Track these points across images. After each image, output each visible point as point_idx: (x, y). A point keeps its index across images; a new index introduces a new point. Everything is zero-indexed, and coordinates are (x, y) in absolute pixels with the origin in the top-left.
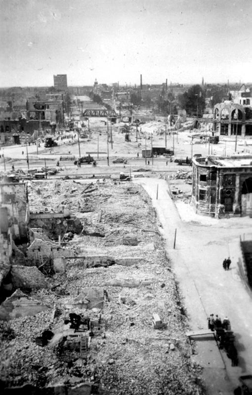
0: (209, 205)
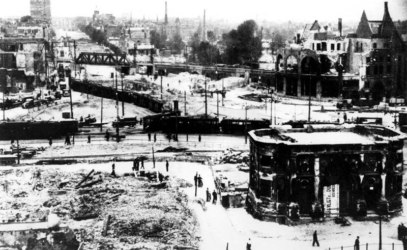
0: (275, 205)
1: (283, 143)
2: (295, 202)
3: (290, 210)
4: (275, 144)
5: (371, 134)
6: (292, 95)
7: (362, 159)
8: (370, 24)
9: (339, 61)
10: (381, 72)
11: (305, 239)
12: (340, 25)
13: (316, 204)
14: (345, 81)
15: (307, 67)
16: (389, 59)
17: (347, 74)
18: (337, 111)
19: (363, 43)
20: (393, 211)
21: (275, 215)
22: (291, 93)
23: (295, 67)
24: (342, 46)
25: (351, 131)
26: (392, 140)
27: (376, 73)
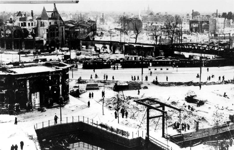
0: (7, 105)
1: (10, 74)
2: (17, 103)
3: (15, 107)
4: (5, 75)
5: (54, 66)
6: (10, 49)
7: (50, 79)
8: (48, 13)
9: (33, 31)
10: (54, 36)
11: (23, 120)
12: (32, 13)
13: (28, 103)
14: (36, 41)
15: (16, 34)
16: (57, 30)
17: (37, 38)
18: (33, 56)
19: (44, 22)
20: (66, 102)
21: (7, 111)
22: (9, 48)
23: (10, 35)
24: (34, 24)
25: (43, 65)
26: (64, 68)
27: (51, 36)
